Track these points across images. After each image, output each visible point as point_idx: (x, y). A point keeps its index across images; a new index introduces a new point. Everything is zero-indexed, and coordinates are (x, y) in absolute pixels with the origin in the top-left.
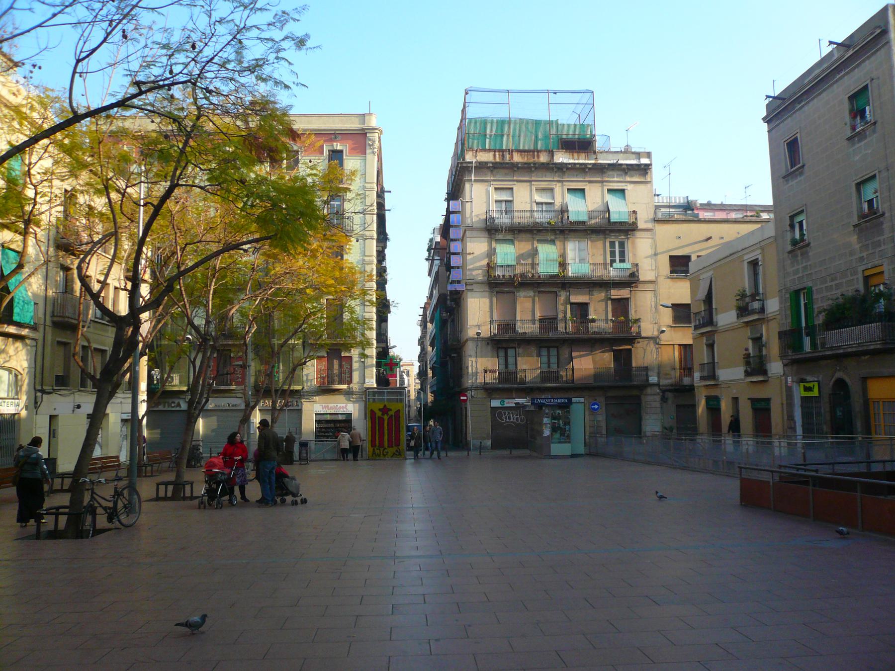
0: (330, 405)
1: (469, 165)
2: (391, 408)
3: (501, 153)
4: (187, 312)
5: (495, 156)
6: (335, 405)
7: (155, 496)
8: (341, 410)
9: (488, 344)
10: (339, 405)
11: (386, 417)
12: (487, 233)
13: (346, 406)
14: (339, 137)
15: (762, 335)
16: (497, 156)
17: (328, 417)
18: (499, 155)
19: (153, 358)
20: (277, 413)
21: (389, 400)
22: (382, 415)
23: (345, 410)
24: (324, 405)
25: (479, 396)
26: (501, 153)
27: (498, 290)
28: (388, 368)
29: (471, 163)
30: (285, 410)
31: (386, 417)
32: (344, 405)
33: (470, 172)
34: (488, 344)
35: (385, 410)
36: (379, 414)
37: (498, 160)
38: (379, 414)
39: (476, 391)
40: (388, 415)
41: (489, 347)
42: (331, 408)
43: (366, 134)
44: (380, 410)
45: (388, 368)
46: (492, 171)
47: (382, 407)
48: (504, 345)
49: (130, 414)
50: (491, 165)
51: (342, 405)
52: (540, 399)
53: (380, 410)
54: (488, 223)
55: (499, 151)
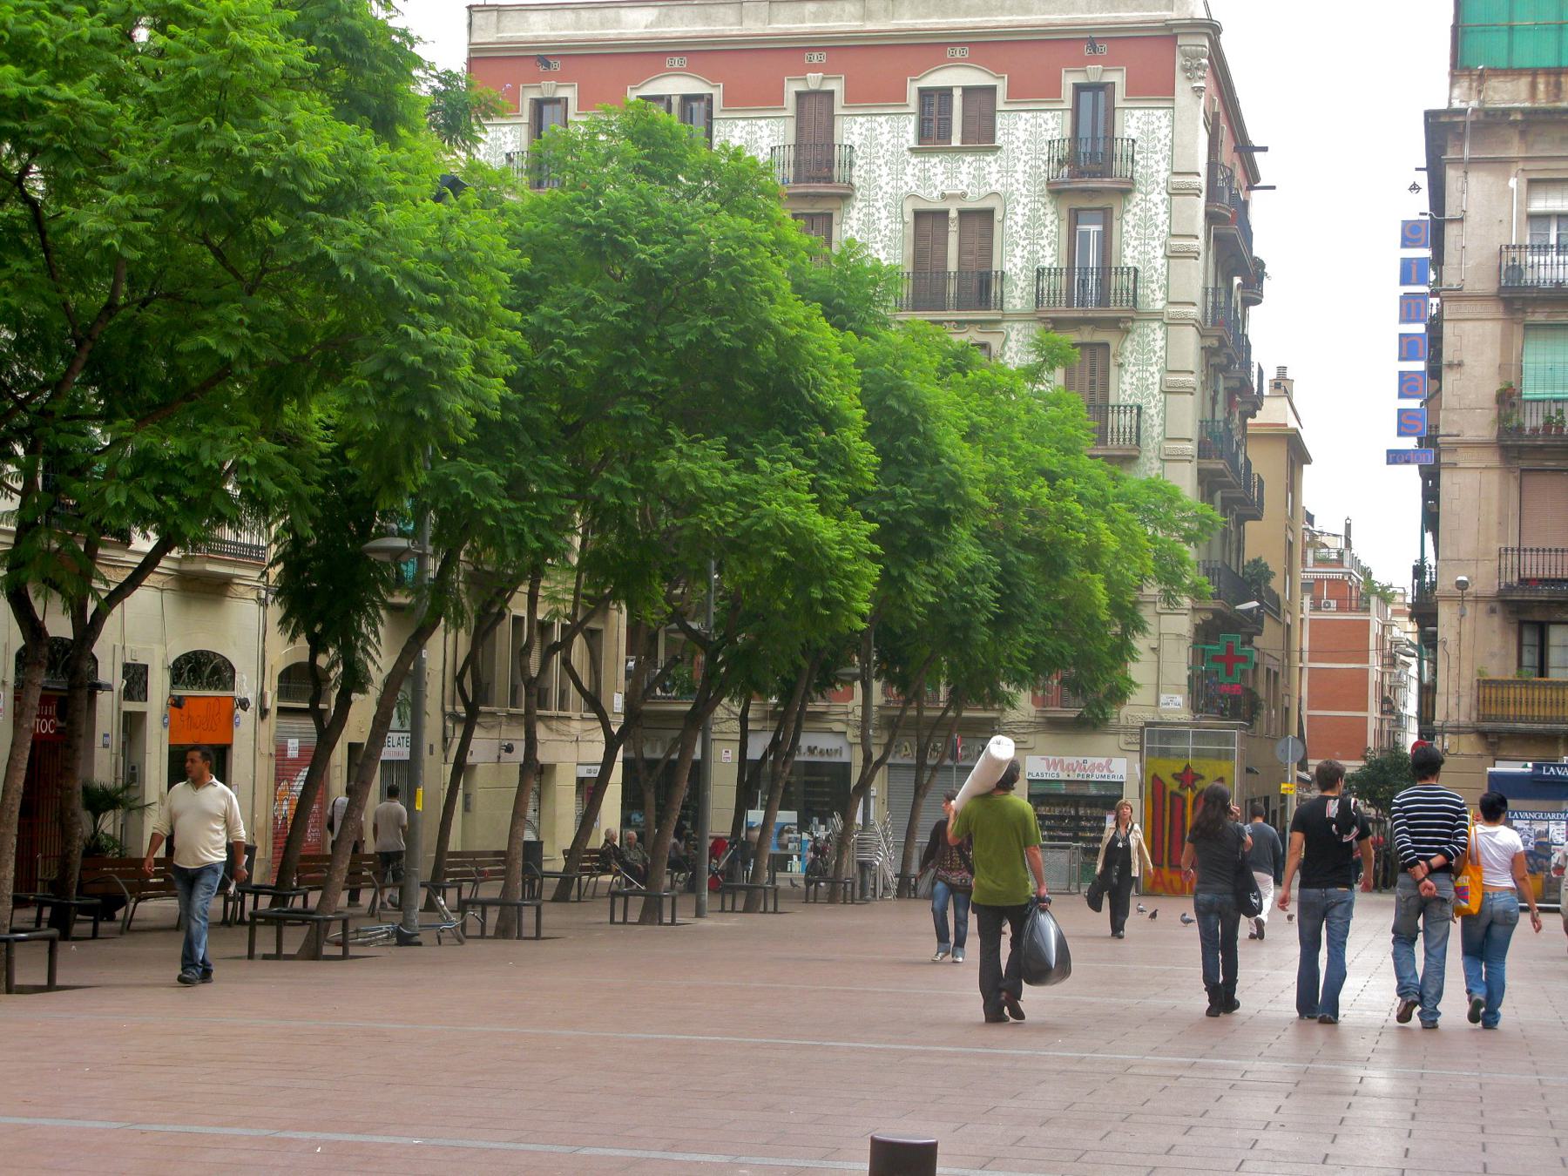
0: (1068, 760)
1: (1456, 119)
2: (1202, 772)
3: (1552, 79)
4: (344, 704)
5: (1533, 87)
6: (1081, 760)
7: (221, 918)
8: (1096, 773)
9: (1493, 611)
10: (1090, 760)
11: (1189, 795)
12: (1501, 309)
13: (1109, 763)
14: (1104, 48)
15: (972, 768)
16: (1541, 87)
17: (1063, 789)
18: (1547, 84)
19: (672, 614)
20: (927, 774)
21: (1198, 754)
22: (1181, 787)
23: (1105, 772)
24: (1051, 758)
25: (1465, 749)
26: (1552, 79)
27: (1525, 464)
28: (1221, 667)
29: (1463, 112)
30: (950, 768)
31: (1189, 795)
32: (1103, 761)
33: (1460, 137)
34: (1493, 611)
35: (1187, 778)
36: (1173, 785)
37: (1542, 102)
38: (1173, 785)
39: (1455, 738)
40: (1193, 789)
41: (1496, 621)
42: (1070, 768)
43: (1175, 37)
44: (1175, 776)
45: (1221, 667)
46: (1523, 134)
47: (1179, 769)
48: (1538, 616)
49: (599, 768)
50: (1519, 117)
51: (1098, 760)
52: (1554, 766)
53: (1175, 776)
54: (1503, 282)
55: (1548, 72)
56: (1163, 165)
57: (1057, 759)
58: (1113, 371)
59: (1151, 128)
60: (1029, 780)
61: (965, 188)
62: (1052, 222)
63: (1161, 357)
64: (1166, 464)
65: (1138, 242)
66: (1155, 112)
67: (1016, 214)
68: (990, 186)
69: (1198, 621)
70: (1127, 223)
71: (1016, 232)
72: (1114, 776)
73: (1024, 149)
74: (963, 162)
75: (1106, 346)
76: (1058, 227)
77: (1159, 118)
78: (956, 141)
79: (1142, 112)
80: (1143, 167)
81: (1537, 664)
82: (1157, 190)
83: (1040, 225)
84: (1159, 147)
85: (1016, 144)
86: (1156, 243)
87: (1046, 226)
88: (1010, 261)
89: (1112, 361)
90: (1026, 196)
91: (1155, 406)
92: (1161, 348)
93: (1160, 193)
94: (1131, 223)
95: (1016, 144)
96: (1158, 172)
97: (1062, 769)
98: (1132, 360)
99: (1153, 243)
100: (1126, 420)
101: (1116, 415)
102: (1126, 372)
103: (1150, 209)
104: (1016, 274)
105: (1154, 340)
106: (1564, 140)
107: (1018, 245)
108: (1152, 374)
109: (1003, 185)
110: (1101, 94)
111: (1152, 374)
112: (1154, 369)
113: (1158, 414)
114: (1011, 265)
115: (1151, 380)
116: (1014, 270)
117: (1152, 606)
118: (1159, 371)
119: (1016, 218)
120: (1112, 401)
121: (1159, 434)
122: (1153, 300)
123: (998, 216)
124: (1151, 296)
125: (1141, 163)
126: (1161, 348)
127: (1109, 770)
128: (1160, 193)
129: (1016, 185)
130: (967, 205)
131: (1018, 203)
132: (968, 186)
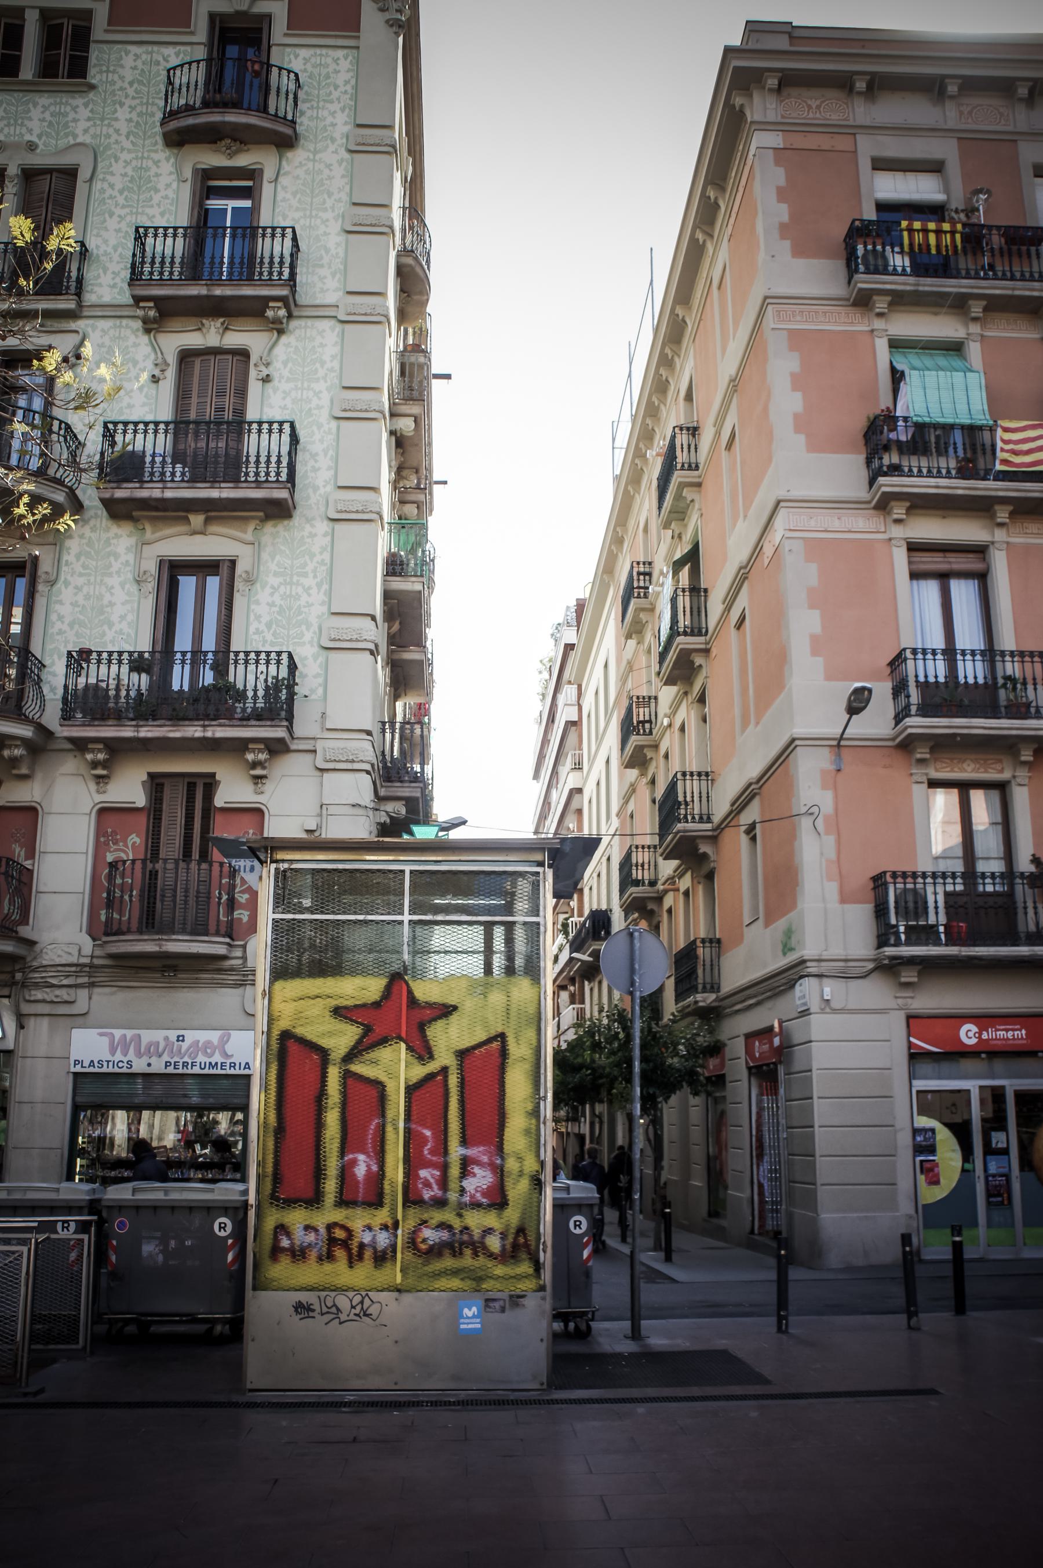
0: (149, 1036)
6: (173, 1035)
10: (191, 1036)
13: (224, 1041)
23: (217, 1058)
32: (214, 1036)
42: (152, 1049)
56: (318, 597)
57: (129, 1033)
58: (254, 387)
59: (324, 72)
60: (75, 1074)
61: (34, 139)
62: (146, 357)
63: (332, 370)
64: (338, 526)
65: (291, 385)
66: (330, 52)
67: (112, 174)
68: (75, 136)
69: (384, 818)
70: (258, 618)
71: (111, 197)
72: (233, 1065)
73: (131, 92)
74: (35, 105)
75: (243, 354)
76: (177, 191)
77: (336, 61)
78: (28, 71)
79: (311, 51)
80: (311, 118)
81: (999, 819)
82: (332, 148)
83: (149, 190)
84: (336, 94)
85: (119, 84)
86: (329, 215)
87: (157, 191)
88: (98, 235)
89: (253, 373)
90: (129, 151)
91: (321, 441)
92: (323, 549)
93: (336, 152)
94: (265, 619)
95: (119, 84)
96: (333, 125)
97: (139, 1055)
98: (286, 373)
99: (325, 216)
100: (282, 247)
101: (268, 240)
102: (275, 390)
103: (320, 172)
104: (106, 253)
105: (322, 345)
106: (1038, 535)
107: (111, 215)
108: (317, 394)
109: (94, 136)
110: (213, 583)
111: (317, 394)
112: (321, 386)
113: (319, 585)
114: (99, 241)
115: (315, 401)
116: (103, 248)
117: (309, 757)
118: (328, 389)
119: (117, 125)
120: (251, 414)
121: (327, 483)
122: (322, 291)
123: (83, 174)
124: (319, 285)
125: (309, 113)
126: (333, 357)
127: (226, 1055)
128: (336, 152)
129: (115, 136)
130: (37, 160)
131: (117, 159)
132: (40, 136)
